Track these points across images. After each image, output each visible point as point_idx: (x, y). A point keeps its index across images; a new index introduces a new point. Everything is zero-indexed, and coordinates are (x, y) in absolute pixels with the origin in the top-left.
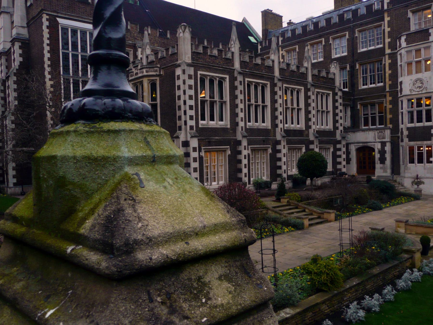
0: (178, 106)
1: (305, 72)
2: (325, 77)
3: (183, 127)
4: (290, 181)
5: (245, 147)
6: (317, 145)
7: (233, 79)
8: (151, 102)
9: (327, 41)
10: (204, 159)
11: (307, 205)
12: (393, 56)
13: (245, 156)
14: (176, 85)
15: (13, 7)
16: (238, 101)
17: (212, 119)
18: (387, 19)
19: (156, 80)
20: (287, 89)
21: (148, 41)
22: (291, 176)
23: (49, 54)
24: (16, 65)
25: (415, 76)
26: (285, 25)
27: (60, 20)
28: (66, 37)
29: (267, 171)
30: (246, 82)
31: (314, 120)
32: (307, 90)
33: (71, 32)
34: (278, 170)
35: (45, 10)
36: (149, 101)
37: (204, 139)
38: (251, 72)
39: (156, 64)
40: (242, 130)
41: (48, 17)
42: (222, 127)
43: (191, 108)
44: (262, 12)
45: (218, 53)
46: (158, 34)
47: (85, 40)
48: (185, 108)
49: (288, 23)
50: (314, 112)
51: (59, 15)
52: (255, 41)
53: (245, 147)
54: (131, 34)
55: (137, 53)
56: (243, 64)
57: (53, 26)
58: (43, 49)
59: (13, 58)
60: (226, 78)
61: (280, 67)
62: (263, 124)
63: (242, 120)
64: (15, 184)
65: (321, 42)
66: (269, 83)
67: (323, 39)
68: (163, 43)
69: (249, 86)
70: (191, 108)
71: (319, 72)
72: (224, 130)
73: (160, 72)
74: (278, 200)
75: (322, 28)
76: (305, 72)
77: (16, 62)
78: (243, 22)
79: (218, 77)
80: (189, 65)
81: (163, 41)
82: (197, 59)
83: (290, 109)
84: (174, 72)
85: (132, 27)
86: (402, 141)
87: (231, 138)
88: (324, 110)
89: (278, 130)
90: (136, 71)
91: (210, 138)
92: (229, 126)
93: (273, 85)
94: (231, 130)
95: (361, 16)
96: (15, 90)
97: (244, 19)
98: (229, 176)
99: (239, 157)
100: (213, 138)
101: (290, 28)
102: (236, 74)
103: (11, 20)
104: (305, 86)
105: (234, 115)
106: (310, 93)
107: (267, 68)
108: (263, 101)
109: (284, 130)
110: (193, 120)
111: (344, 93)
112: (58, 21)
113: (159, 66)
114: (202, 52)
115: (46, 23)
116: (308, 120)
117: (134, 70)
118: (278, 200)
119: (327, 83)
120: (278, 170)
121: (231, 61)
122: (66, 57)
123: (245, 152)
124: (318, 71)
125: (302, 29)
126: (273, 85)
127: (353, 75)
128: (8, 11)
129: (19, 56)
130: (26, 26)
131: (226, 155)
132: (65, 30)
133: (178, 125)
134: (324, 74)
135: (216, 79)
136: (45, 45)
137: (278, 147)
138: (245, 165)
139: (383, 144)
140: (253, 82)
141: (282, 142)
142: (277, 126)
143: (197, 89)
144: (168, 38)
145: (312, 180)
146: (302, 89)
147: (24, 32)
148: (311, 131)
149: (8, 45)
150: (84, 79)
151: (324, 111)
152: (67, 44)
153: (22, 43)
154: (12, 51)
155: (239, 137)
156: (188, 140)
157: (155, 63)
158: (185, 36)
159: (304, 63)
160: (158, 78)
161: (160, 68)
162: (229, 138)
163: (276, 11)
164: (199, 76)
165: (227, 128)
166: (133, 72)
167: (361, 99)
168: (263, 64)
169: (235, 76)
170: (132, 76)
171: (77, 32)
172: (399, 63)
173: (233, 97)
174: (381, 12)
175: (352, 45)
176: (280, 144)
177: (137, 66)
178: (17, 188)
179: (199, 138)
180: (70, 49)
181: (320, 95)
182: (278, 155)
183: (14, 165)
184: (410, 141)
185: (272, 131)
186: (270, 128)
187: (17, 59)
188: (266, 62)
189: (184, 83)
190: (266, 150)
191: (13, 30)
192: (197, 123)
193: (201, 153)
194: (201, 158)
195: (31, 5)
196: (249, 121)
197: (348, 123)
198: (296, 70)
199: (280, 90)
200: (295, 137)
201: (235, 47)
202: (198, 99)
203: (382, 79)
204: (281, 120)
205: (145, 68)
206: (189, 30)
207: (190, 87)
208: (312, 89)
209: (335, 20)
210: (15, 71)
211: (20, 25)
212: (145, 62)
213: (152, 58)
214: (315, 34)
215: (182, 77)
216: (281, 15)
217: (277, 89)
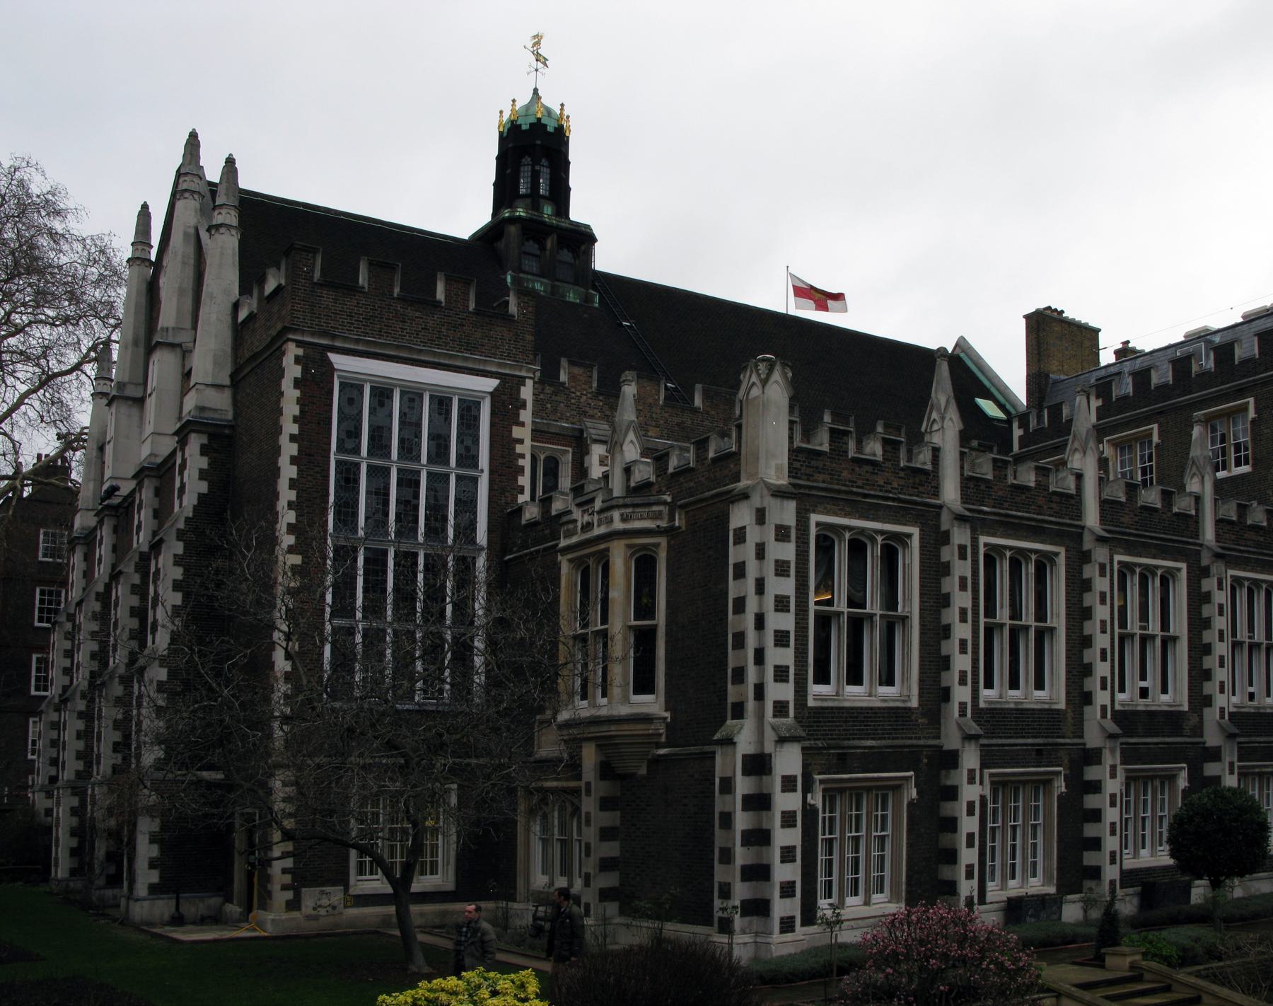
0: (734, 635)
1: (1193, 512)
2: (1262, 528)
3: (751, 705)
4: (1131, 890)
5: (971, 773)
6: (1231, 764)
7: (935, 540)
8: (633, 623)
10: (821, 815)
11: (1206, 977)
13: (971, 806)
14: (731, 561)
15: (195, 328)
16: (951, 616)
19: (657, 545)
20: (1126, 568)
21: (633, 418)
22: (1133, 872)
23: (295, 468)
24: (186, 505)
26: (1107, 357)
27: (337, 360)
28: (355, 412)
29: (1047, 855)
30: (982, 550)
31: (1221, 675)
32: (1198, 573)
33: (388, 447)
34: (1085, 854)
35: (295, 331)
36: (626, 617)
37: (824, 748)
38: (999, 514)
39: (660, 492)
40: (963, 713)
41: (300, 352)
42: (891, 704)
43: (781, 639)
45: (884, 451)
46: (662, 397)
47: (414, 420)
48: (761, 639)
49: (1117, 353)
50: (1221, 649)
51: (338, 344)
52: (1000, 414)
53: (971, 773)
54: (568, 398)
55: (586, 458)
56: (969, 485)
57: (316, 379)
58: (277, 451)
59: (178, 484)
60: (909, 536)
61: (1105, 496)
62: (1038, 693)
64: (153, 889)
65: (1244, 408)
66: (1062, 550)
67: (1251, 400)
68: (678, 424)
70: (781, 639)
71: (1242, 509)
72: (896, 716)
73: (672, 519)
74: (1098, 961)
76: (1193, 512)
77: (142, 534)
78: (958, 351)
79: (882, 532)
80: (779, 493)
81: (677, 420)
82: (809, 471)
83: (1137, 639)
84: (724, 519)
85: (572, 377)
87: (921, 742)
88: (1256, 639)
89: (1092, 714)
90: (587, 518)
91: (846, 743)
92: (914, 703)
93: (1079, 558)
94: (923, 715)
96: (177, 586)
97: (962, 344)
98: (908, 877)
99: (947, 808)
100: (857, 743)
101: (1127, 367)
102: (945, 522)
103: (184, 366)
104: (1190, 555)
105: (935, 663)
106: (1209, 584)
107: (1055, 498)
108: (1041, 614)
109: (1114, 712)
110: (787, 681)
112: (331, 364)
113: (669, 499)
114: (826, 447)
115: (292, 371)
116: (1199, 675)
117: (577, 514)
118: (1098, 961)
120: (1085, 854)
121: (929, 479)
122: (348, 476)
123: (970, 793)
124: (1239, 505)
125: (1174, 370)
126: (1079, 558)
128: (177, 341)
129: (197, 476)
130: (227, 382)
131: (901, 802)
132: (352, 388)
135: (873, 540)
136: (284, 440)
137: (1091, 773)
138: (970, 836)
140: (1005, 547)
142: (1087, 698)
143: (806, 576)
144: (696, 410)
145: (1216, 884)
146: (1179, 570)
147: (221, 402)
148: (1211, 716)
149: (167, 445)
150: (404, 548)
151: (1259, 645)
152: (356, 434)
153: (212, 437)
154: (179, 461)
155: (951, 740)
156: (767, 751)
158: (769, 400)
159: (1187, 479)
160: (663, 541)
161: (672, 507)
162: (914, 742)
163: (1073, 312)
164: (813, 531)
165: (910, 709)
166: (575, 521)
168: (1042, 486)
169: (944, 527)
170: (569, 534)
171: (390, 397)
173: (935, 601)
176: (1099, 762)
177: (592, 500)
178: (160, 903)
179: (807, 744)
181: (1245, 591)
182: (1091, 801)
183: (155, 826)
185: (1070, 715)
186: (1062, 706)
187: (192, 485)
188: (1052, 478)
189: (761, 552)
190: (1047, 782)
191: (187, 399)
192: (801, 691)
193: (809, 796)
194: (809, 813)
195: (251, 317)
196: (989, 684)
198: (1159, 506)
199: (1102, 574)
200: (1153, 738)
201: (945, 431)
202: (807, 611)
204: (1104, 680)
205: (618, 507)
206: (785, 374)
207: (782, 569)
208: (1217, 568)
210: (181, 525)
211: (209, 380)
212: (617, 487)
213: (640, 475)
214: (1222, 384)
215: (753, 536)
216: (1093, 324)
217: (1090, 571)
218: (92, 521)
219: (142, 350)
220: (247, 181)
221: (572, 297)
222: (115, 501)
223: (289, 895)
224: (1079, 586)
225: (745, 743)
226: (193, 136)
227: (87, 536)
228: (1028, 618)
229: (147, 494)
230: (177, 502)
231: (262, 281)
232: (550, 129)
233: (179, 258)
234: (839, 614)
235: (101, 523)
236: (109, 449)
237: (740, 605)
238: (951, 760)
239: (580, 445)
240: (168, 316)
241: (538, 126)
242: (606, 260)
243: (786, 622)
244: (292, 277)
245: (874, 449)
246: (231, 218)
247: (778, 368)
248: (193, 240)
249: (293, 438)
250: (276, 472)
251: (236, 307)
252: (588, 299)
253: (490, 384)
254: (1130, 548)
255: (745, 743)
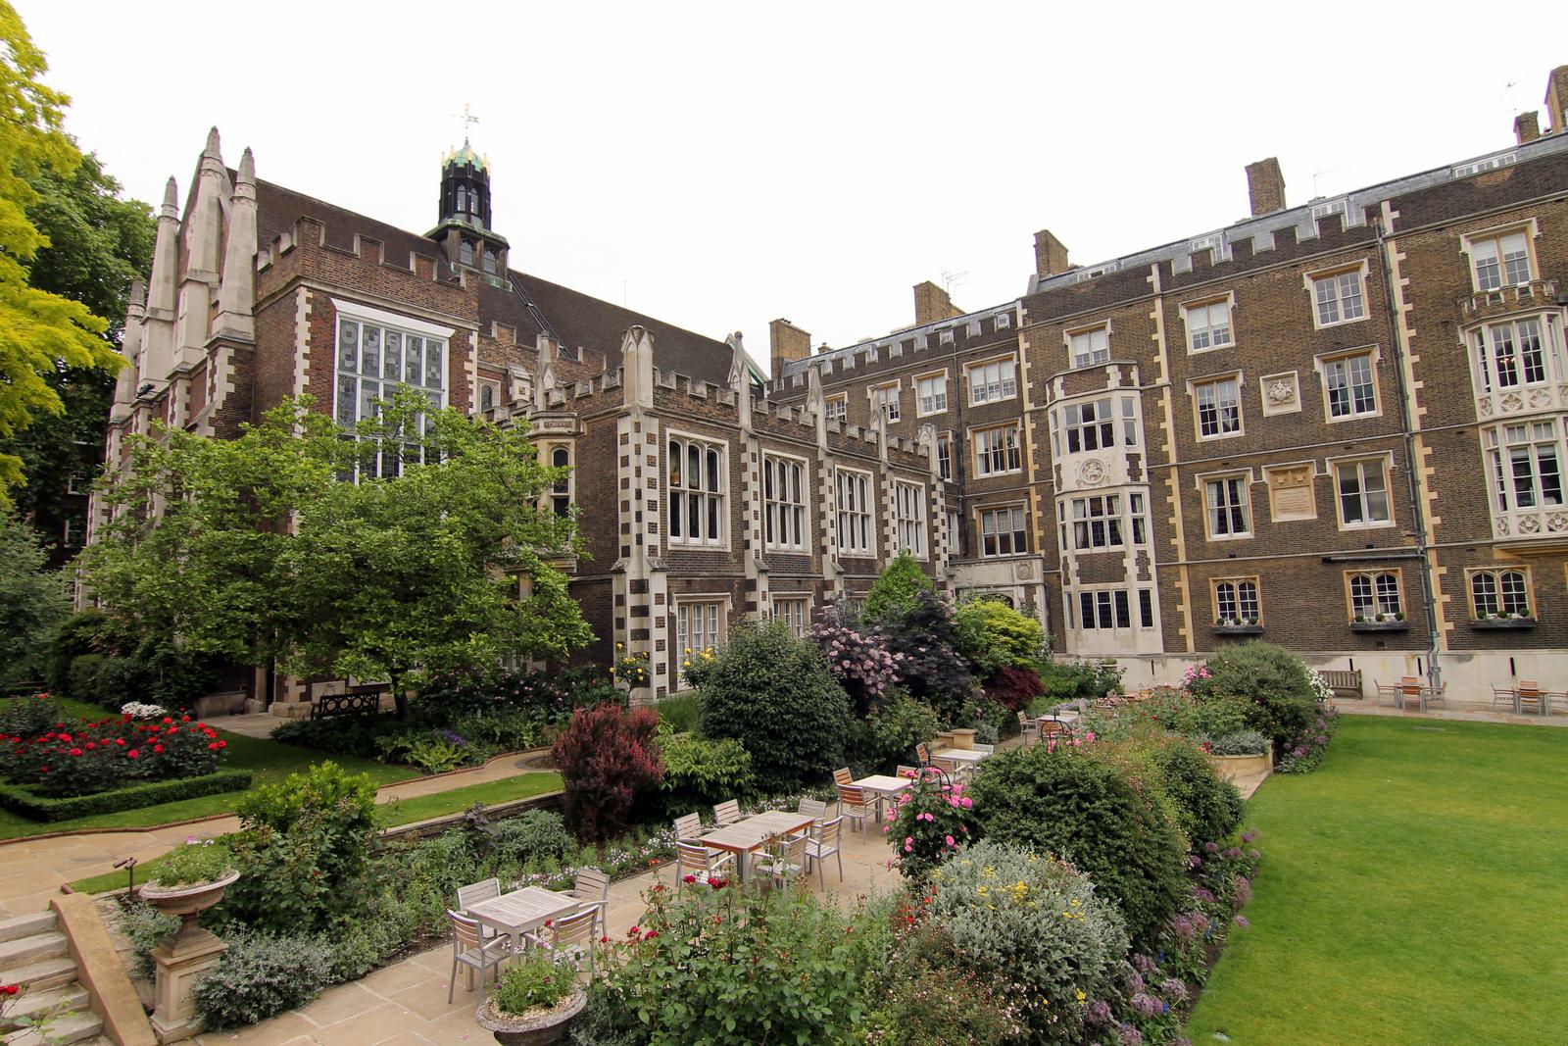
3: (634, 548)
7: (738, 449)
9: (907, 384)
12: (1039, 416)
17: (694, 532)
18: (1023, 346)
25: (1084, 455)
26: (815, 352)
41: (310, 295)
44: (1248, 168)
48: (639, 505)
50: (894, 523)
51: (339, 292)
57: (323, 316)
58: (293, 365)
63: (756, 537)
69: (768, 464)
70: (652, 506)
72: (720, 556)
75: (1352, 231)
84: (615, 427)
86: (1067, 582)
89: (827, 559)
95: (1304, 243)
104: (876, 468)
111: (947, 485)
114: (674, 387)
115: (304, 308)
119: (911, 463)
121: (731, 410)
127: (961, 448)
132: (350, 324)
133: (621, 544)
134: (908, 447)
135: (702, 447)
136: (298, 357)
139: (1030, 588)
141: (837, 584)
142: (824, 550)
147: (246, 327)
149: (195, 359)
153: (237, 351)
157: (565, 408)
158: (639, 353)
160: (572, 441)
161: (578, 419)
167: (979, 499)
171: (378, 334)
172: (1052, 430)
173: (739, 487)
174: (1012, 331)
175: (958, 388)
180: (359, 370)
184: (1082, 582)
187: (222, 383)
189: (638, 451)
192: (664, 540)
194: (672, 618)
195: (268, 267)
197: (955, 547)
203: (1016, 459)
207: (651, 462)
208: (890, 475)
209: (922, 343)
210: (213, 415)
212: (540, 402)
213: (557, 397)
215: (633, 439)
218: (127, 411)
219: (171, 286)
220: (265, 172)
221: (494, 284)
222: (149, 396)
223: (303, 689)
224: (817, 482)
225: (632, 572)
226: (215, 130)
227: (122, 423)
228: (790, 500)
229: (180, 390)
230: (208, 398)
231: (277, 240)
232: (478, 169)
233: (205, 219)
234: (684, 492)
235: (137, 412)
236: (143, 359)
237: (626, 483)
238: (751, 585)
239: (506, 378)
240: (195, 261)
241: (469, 166)
242: (516, 262)
243: (655, 495)
244: (303, 241)
245: (702, 390)
246: (251, 193)
247: (646, 335)
248: (216, 208)
249: (305, 356)
250: (292, 380)
251: (255, 258)
252: (505, 286)
253: (451, 332)
254: (843, 461)
255: (632, 572)
